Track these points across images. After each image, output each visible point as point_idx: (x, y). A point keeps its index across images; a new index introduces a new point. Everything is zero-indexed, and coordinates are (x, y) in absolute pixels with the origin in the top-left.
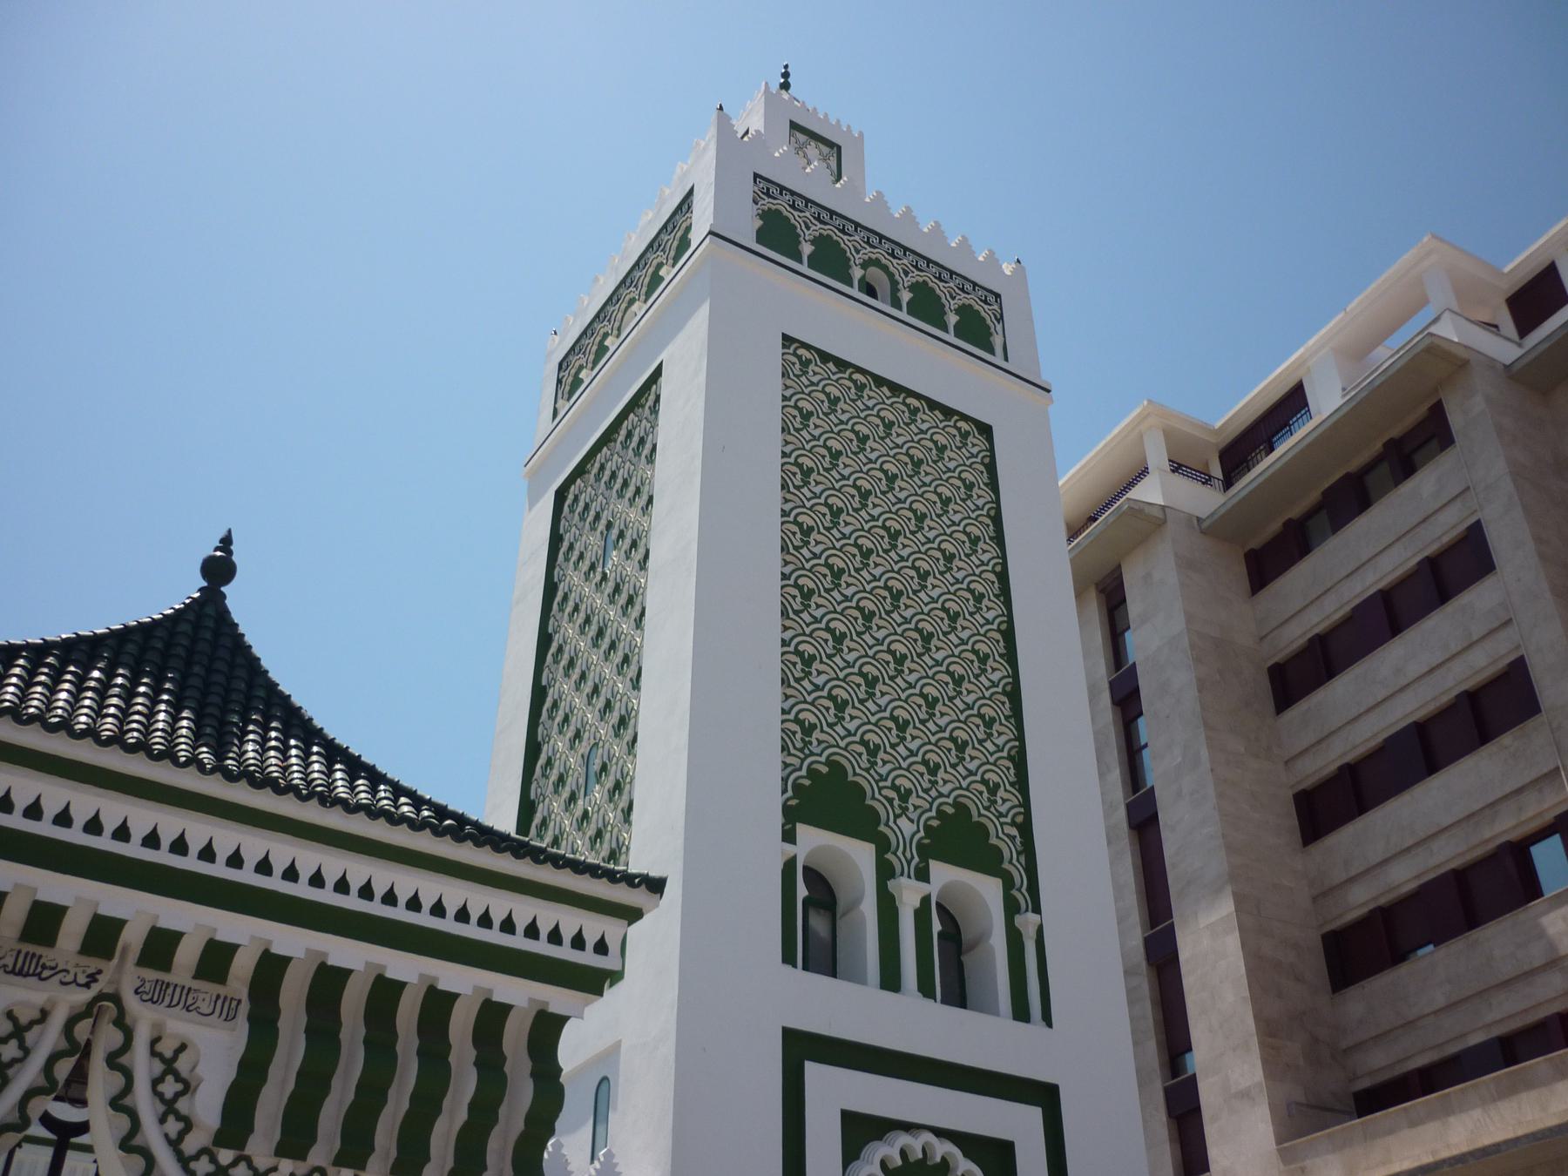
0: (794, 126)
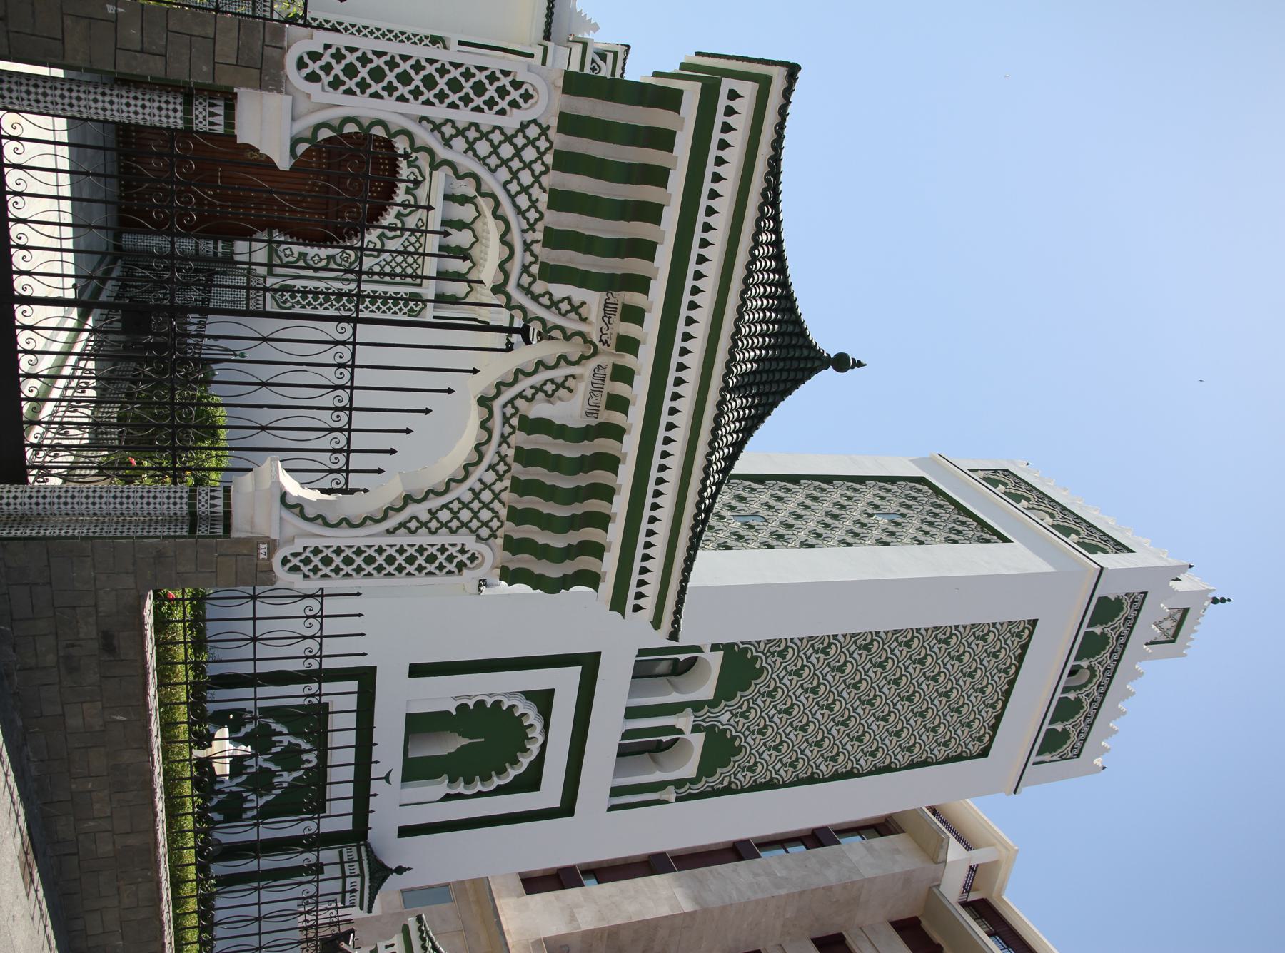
0: (1186, 611)
